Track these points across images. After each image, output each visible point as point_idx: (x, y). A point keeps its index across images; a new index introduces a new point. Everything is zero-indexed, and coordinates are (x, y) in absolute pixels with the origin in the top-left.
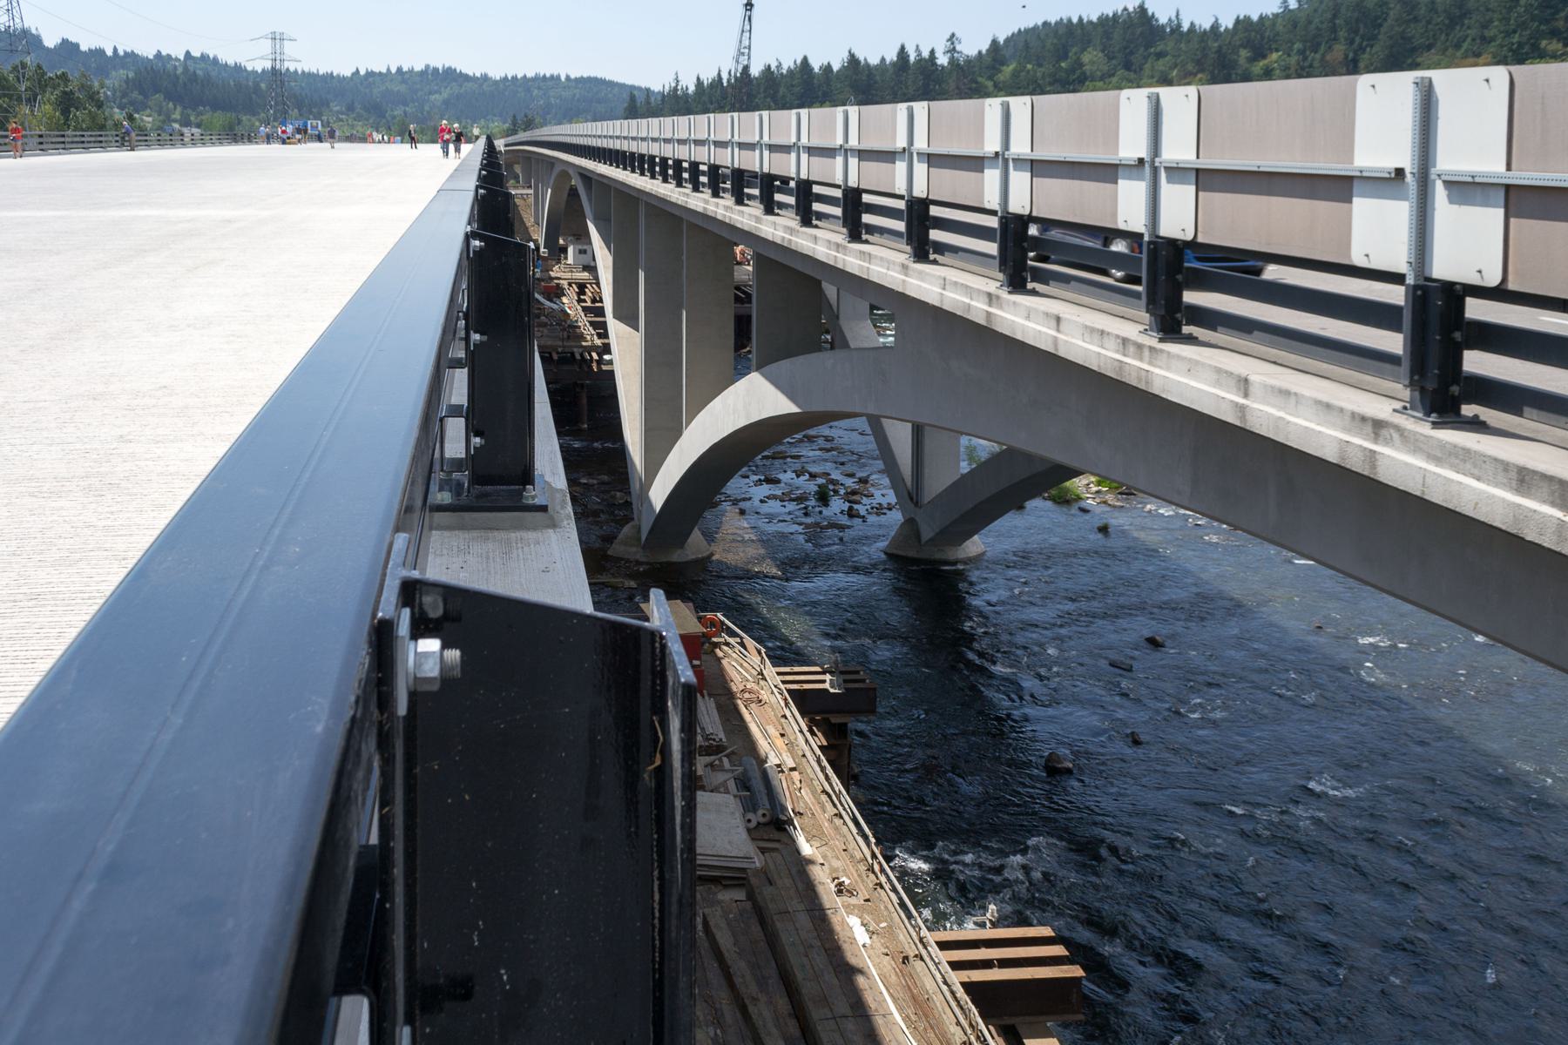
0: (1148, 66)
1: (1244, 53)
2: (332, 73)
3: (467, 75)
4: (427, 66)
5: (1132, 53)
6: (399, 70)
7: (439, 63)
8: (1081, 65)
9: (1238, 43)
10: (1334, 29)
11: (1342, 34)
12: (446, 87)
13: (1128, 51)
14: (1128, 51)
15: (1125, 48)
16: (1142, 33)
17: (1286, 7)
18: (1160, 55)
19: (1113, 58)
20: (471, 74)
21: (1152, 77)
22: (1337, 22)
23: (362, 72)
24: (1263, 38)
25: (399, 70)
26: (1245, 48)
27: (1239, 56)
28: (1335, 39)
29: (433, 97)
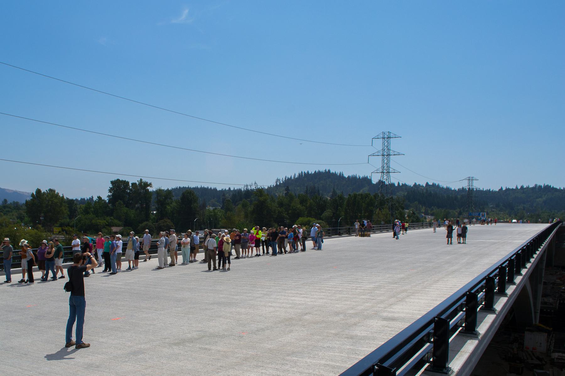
2: (490, 190)
3: (556, 189)
4: (536, 185)
6: (522, 187)
7: (542, 183)
12: (545, 195)
20: (558, 188)
23: (504, 189)
25: (522, 187)
29: (538, 200)
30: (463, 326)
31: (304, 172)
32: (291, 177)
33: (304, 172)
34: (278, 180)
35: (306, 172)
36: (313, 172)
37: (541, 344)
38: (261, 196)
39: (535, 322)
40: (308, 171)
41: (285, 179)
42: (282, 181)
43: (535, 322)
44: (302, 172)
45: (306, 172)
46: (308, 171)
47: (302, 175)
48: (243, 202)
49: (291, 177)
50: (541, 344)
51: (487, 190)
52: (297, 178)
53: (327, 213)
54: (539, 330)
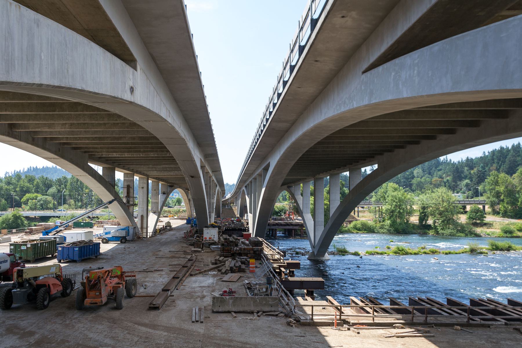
0: (435, 173)
1: (466, 168)
5: (431, 169)
8: (413, 173)
9: (464, 165)
10: (493, 159)
11: (496, 161)
13: (430, 169)
14: (430, 169)
15: (429, 168)
16: (434, 163)
17: (485, 154)
18: (441, 170)
19: (426, 171)
21: (437, 177)
22: (494, 157)
24: (473, 164)
26: (466, 167)
27: (464, 169)
28: (494, 163)
30: (469, 321)
31: (33, 167)
32: (20, 171)
33: (33, 167)
34: (7, 173)
35: (35, 167)
36: (41, 167)
37: (214, 235)
38: (291, 276)
39: (253, 236)
40: (36, 167)
41: (15, 172)
42: (12, 174)
43: (253, 236)
44: (31, 167)
45: (35, 167)
46: (36, 167)
47: (31, 169)
48: (490, 200)
49: (20, 171)
50: (214, 235)
51: (496, 149)
52: (26, 171)
53: (53, 190)
54: (213, 226)
